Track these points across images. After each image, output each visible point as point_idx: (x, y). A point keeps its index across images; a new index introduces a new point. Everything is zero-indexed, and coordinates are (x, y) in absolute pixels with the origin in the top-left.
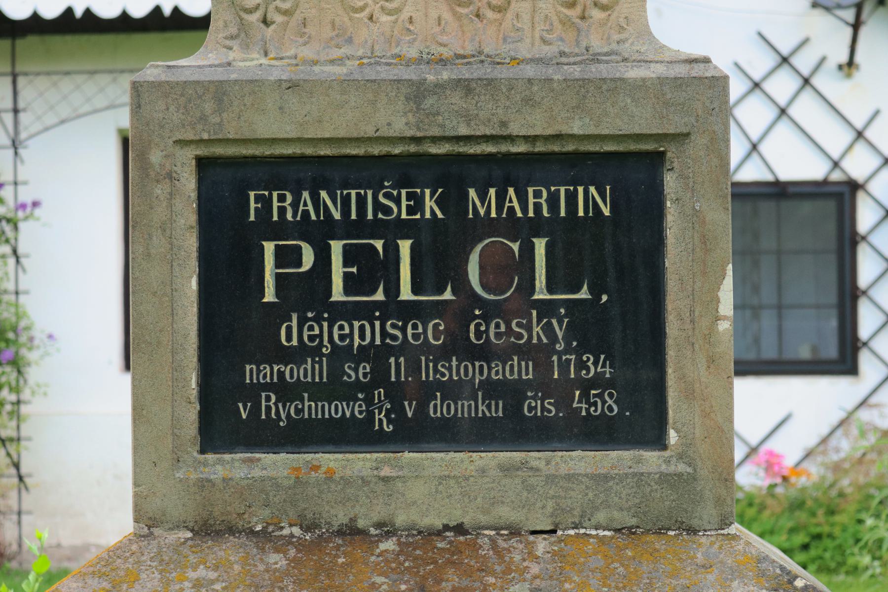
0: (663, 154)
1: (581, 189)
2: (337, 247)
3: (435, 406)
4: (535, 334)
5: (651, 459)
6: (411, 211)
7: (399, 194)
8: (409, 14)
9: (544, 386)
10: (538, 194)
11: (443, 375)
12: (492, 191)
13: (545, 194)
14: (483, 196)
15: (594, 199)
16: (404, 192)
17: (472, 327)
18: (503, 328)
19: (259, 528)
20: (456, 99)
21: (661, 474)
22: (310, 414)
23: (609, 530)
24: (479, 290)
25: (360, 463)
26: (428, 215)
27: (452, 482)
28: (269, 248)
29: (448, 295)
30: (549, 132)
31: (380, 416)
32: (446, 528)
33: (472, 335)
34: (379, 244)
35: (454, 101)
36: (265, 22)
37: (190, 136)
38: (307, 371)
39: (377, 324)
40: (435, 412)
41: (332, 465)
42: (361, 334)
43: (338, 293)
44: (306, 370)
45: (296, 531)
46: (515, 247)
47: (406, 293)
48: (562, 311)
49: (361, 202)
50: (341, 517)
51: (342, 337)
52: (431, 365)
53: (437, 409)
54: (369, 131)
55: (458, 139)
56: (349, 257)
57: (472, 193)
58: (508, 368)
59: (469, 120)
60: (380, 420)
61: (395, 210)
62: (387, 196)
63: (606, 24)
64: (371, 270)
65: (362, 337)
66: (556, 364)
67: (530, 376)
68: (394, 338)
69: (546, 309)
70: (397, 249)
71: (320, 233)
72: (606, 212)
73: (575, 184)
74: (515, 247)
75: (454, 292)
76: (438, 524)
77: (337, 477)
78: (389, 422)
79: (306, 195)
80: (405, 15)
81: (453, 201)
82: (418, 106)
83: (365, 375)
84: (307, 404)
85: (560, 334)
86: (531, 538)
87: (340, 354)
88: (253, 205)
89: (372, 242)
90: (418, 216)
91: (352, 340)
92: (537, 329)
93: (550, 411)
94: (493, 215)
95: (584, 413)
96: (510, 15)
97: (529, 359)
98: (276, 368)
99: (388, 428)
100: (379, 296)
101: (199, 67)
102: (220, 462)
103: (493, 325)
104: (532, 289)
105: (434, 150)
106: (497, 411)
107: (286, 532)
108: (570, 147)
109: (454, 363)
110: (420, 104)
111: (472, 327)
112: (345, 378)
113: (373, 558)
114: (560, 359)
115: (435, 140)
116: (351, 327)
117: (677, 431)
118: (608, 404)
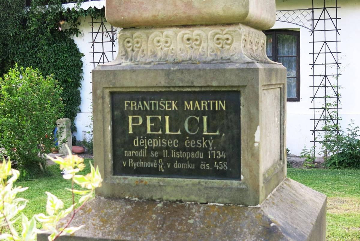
0: (240, 91)
1: (217, 102)
2: (148, 118)
3: (176, 165)
4: (203, 145)
5: (235, 183)
6: (169, 107)
7: (165, 102)
8: (172, 48)
9: (206, 159)
10: (204, 103)
11: (178, 156)
12: (191, 102)
13: (206, 103)
14: (189, 103)
15: (221, 105)
16: (167, 102)
17: (186, 142)
18: (194, 143)
19: (127, 197)
20: (179, 75)
21: (238, 188)
22: (142, 166)
23: (223, 204)
24: (187, 131)
25: (154, 180)
26: (173, 109)
27: (178, 188)
28: (130, 117)
29: (179, 133)
30: (206, 85)
31: (161, 167)
32: (177, 200)
33: (186, 145)
34: (160, 117)
35: (178, 75)
36: (133, 50)
37: (107, 86)
38: (141, 154)
39: (160, 140)
40: (176, 166)
41: (146, 181)
42: (155, 143)
43: (149, 132)
44: (141, 153)
45: (137, 199)
46: (198, 119)
47: (167, 132)
48: (211, 138)
49: (155, 104)
50: (148, 196)
51: (150, 144)
52: (174, 153)
53: (177, 166)
54: (154, 84)
55: (180, 87)
56: (152, 120)
57: (186, 103)
58: (196, 155)
59: (182, 80)
60: (161, 168)
61: (164, 107)
62: (162, 103)
63: (229, 49)
64: (158, 125)
65: (156, 144)
66: (210, 154)
67: (202, 157)
68: (164, 144)
69: (207, 137)
70: (165, 118)
71: (144, 113)
72: (224, 108)
73: (215, 100)
74: (198, 119)
75: (181, 131)
76: (175, 199)
77: (147, 184)
78: (163, 169)
79: (140, 103)
80: (171, 48)
81: (180, 105)
82: (168, 77)
83: (156, 155)
84: (141, 163)
85: (211, 145)
86: (200, 205)
87: (150, 149)
88: (126, 105)
89: (158, 116)
90: (170, 109)
91: (153, 145)
92: (204, 143)
93: (208, 168)
94: (192, 109)
95: (217, 169)
96: (201, 47)
97: (173, 158)
98: (133, 152)
99: (163, 171)
100: (160, 132)
101: (111, 65)
102: (117, 178)
103: (192, 142)
104: (203, 131)
105: (173, 90)
106: (193, 167)
107: (134, 199)
108: (212, 89)
109: (181, 152)
110: (169, 76)
111: (186, 142)
112: (151, 156)
113: (154, 209)
114: (211, 152)
115: (174, 87)
116: (153, 141)
117: (243, 175)
118: (224, 166)
